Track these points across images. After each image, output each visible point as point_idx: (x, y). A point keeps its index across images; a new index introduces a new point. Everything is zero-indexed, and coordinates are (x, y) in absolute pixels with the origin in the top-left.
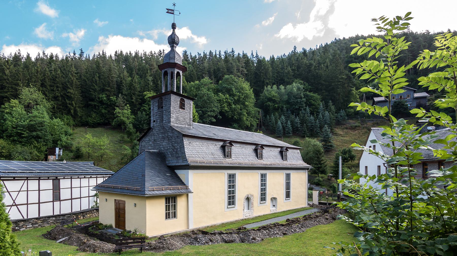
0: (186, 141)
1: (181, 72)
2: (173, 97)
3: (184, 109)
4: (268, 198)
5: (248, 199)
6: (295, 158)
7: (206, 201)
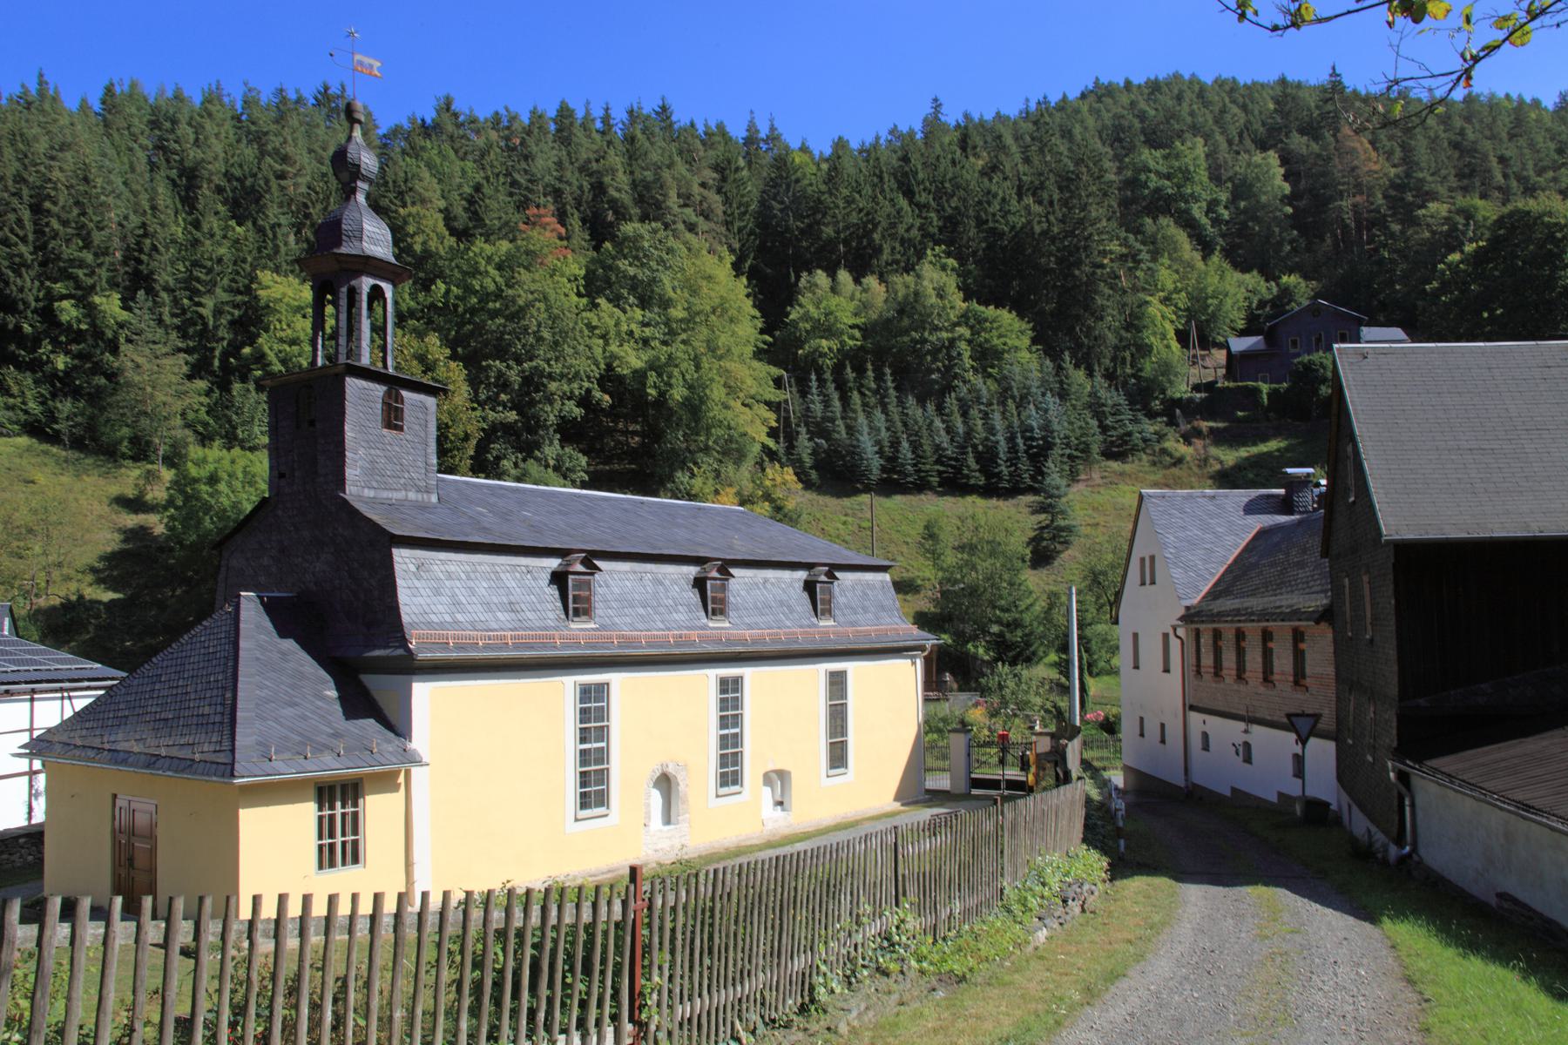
0: (403, 558)
1: (388, 288)
2: (353, 385)
3: (401, 429)
4: (752, 768)
5: (665, 782)
6: (866, 599)
7: (480, 803)
